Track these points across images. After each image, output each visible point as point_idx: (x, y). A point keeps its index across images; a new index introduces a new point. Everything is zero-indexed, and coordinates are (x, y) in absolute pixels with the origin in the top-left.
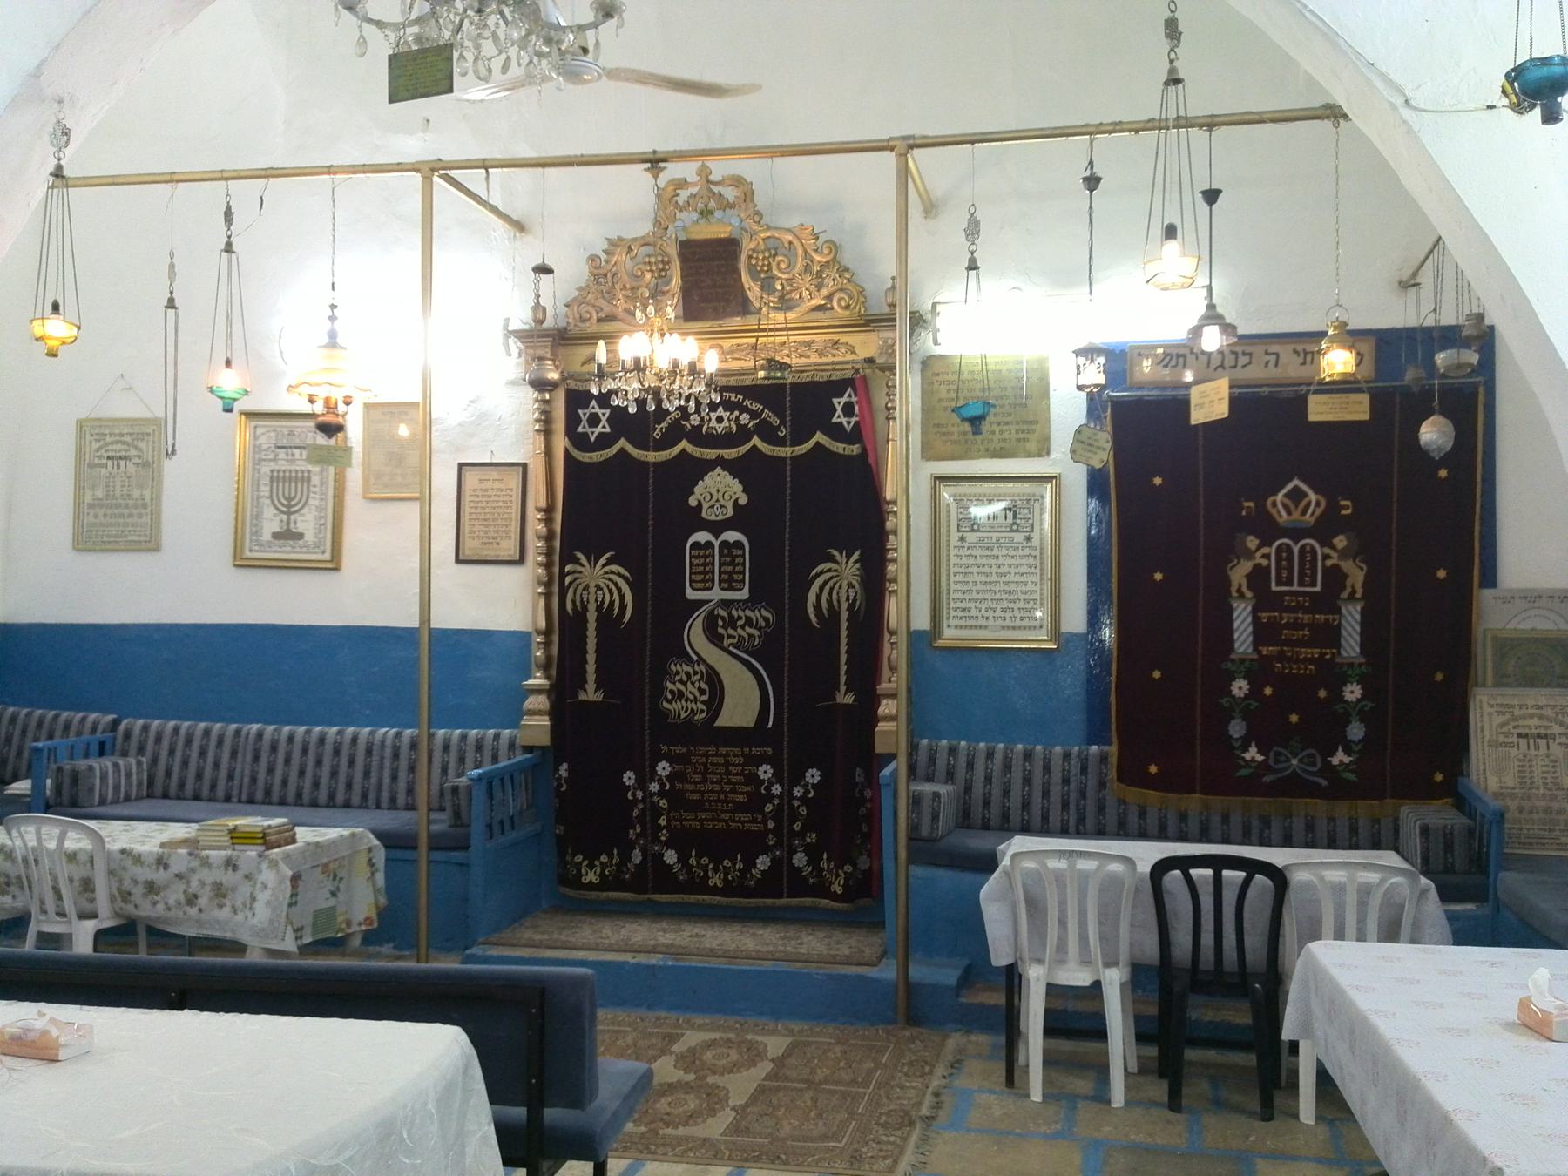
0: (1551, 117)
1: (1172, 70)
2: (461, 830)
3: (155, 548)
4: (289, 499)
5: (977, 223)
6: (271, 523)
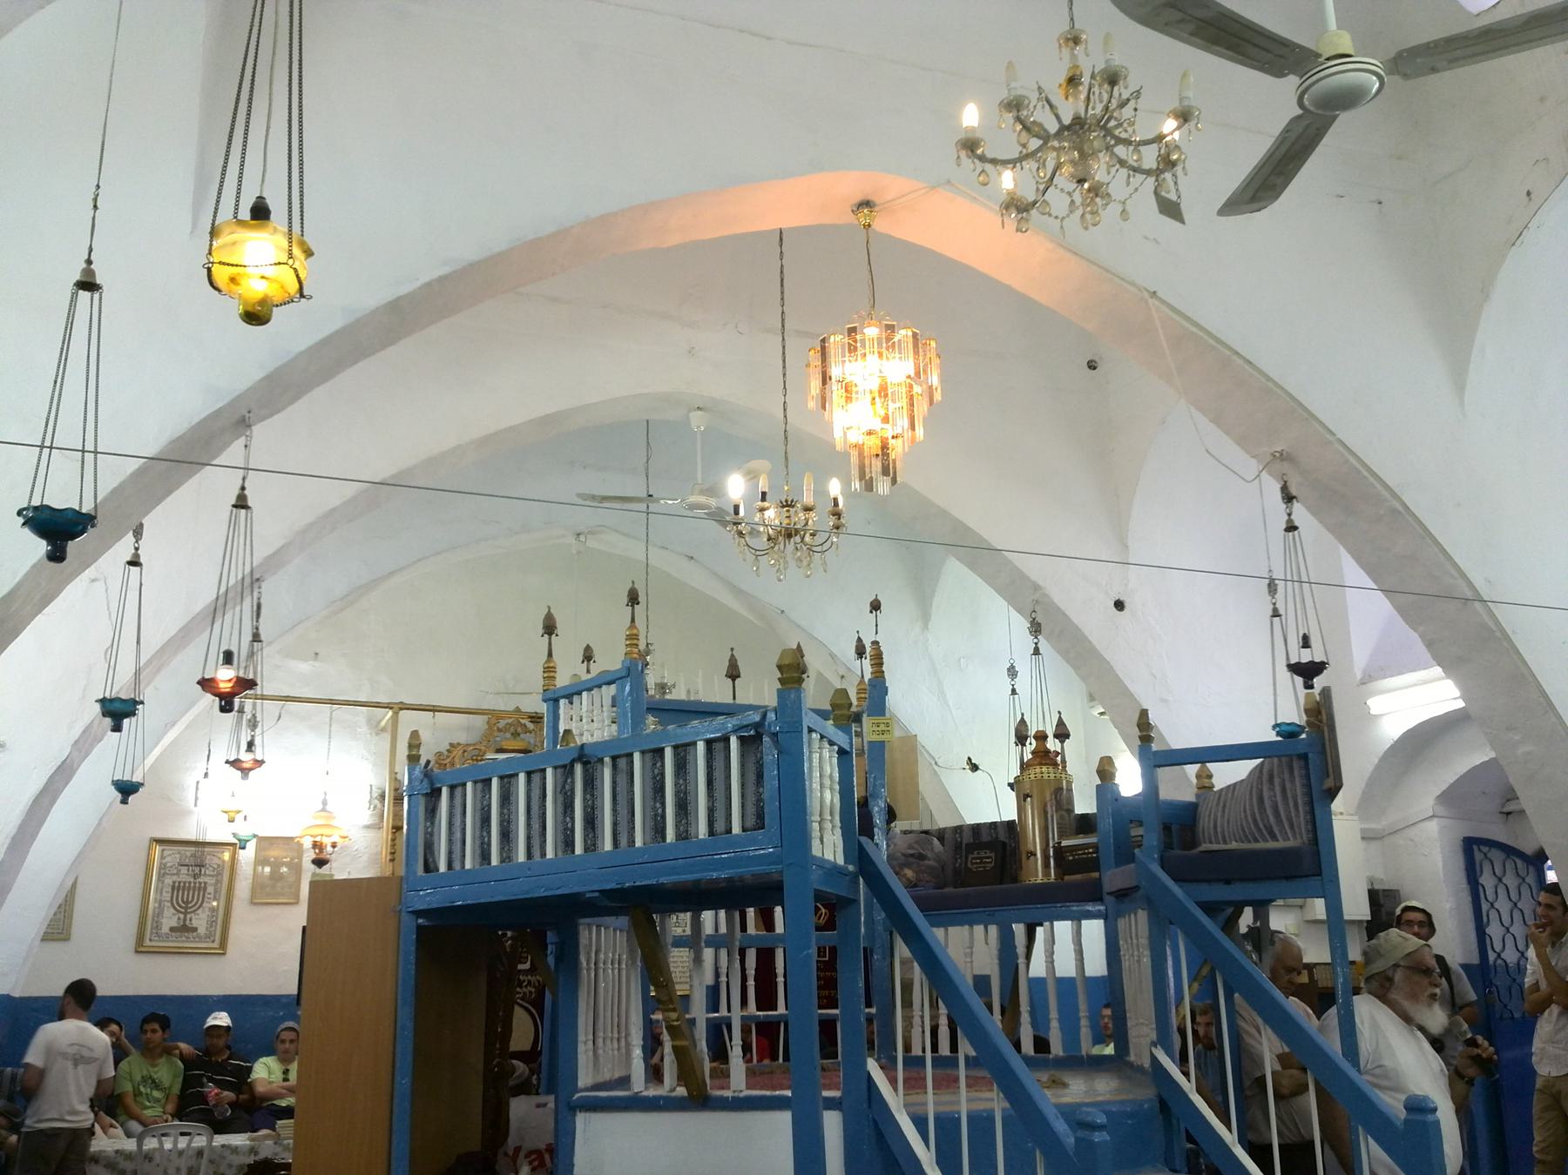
0: (117, 728)
1: (1290, 521)
2: (1046, 771)
3: (67, 939)
4: (187, 903)
6: (170, 920)
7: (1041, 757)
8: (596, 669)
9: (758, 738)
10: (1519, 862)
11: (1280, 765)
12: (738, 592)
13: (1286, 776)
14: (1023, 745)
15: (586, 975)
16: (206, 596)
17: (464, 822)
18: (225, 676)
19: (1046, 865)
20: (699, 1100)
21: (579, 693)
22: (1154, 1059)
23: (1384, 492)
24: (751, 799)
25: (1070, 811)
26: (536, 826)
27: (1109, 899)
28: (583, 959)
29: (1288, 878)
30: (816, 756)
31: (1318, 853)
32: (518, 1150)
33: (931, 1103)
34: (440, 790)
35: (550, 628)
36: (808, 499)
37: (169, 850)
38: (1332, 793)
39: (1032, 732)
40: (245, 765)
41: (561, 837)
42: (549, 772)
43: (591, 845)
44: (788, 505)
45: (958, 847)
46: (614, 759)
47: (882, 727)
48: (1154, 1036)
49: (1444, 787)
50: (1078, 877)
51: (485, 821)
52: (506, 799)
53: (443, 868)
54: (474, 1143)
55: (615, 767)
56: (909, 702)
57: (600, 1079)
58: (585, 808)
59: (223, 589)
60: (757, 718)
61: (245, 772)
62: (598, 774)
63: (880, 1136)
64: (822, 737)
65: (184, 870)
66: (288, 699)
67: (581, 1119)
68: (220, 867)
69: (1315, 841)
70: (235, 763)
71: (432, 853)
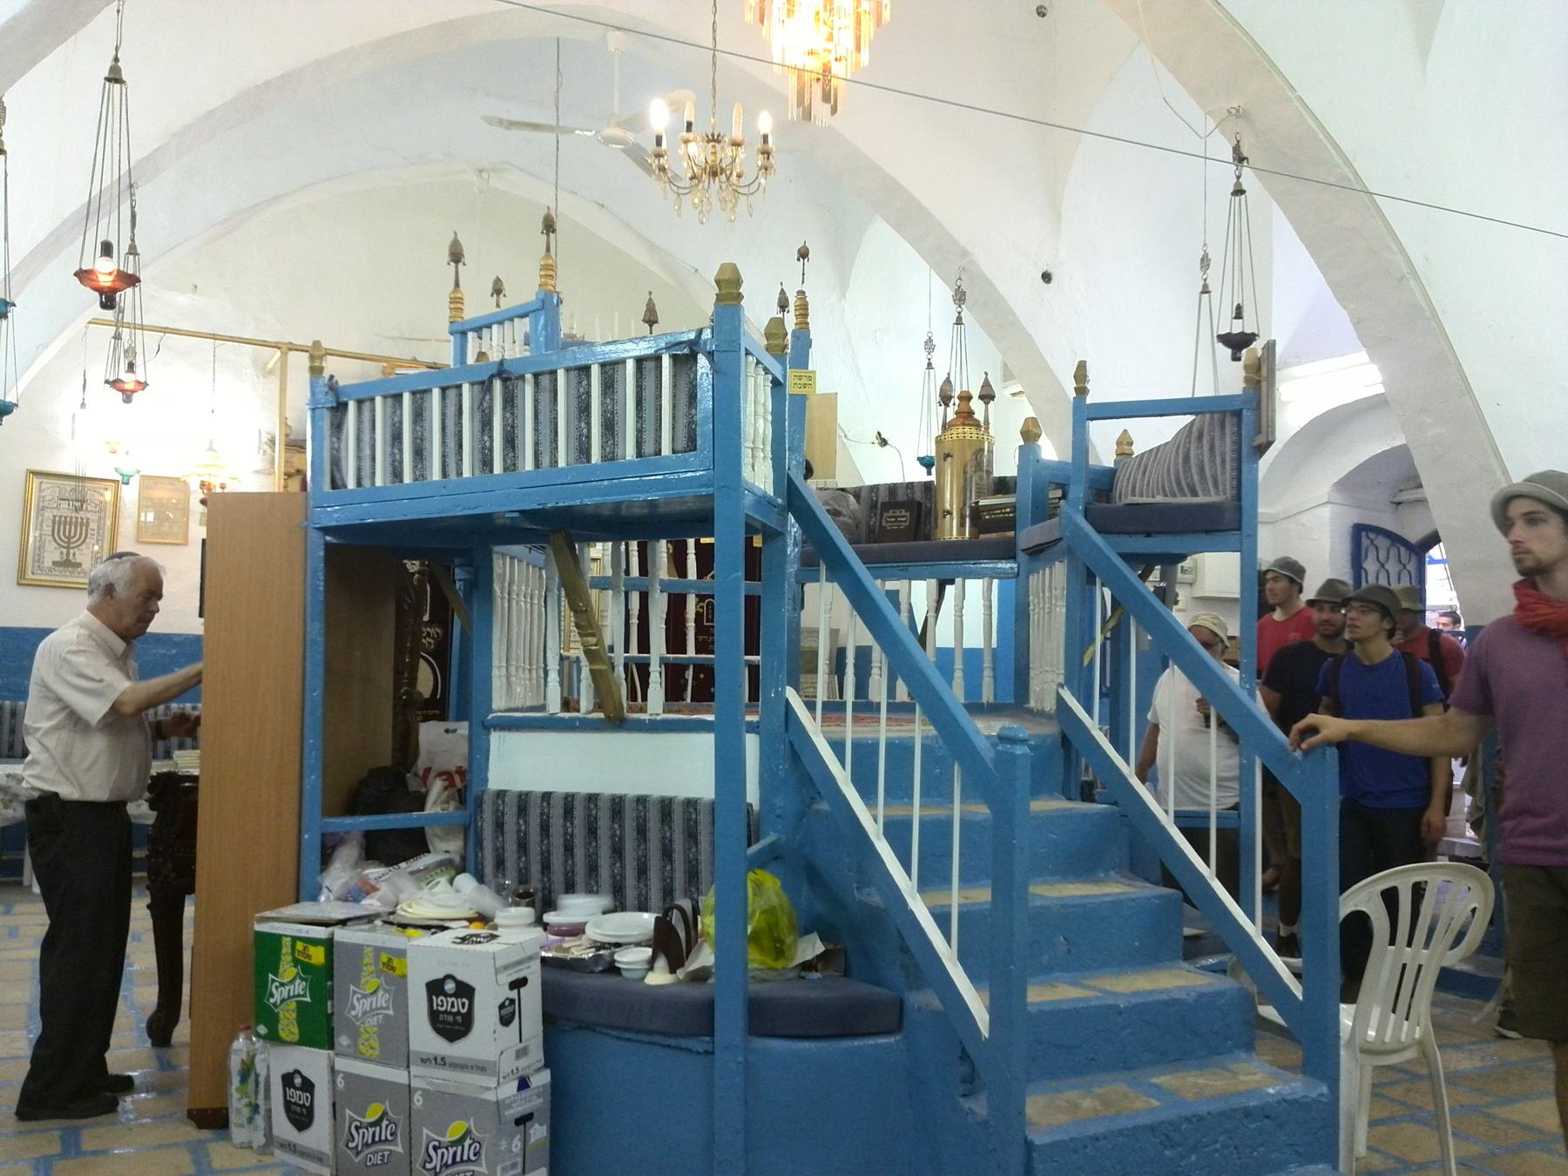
1: (1238, 184)
2: (969, 432)
5: (964, 293)
6: (52, 554)
7: (962, 412)
8: (506, 303)
9: (692, 358)
10: (1403, 550)
11: (1212, 423)
12: (652, 247)
13: (1217, 434)
14: (947, 405)
15: (500, 603)
16: (77, 199)
17: (373, 439)
18: (105, 270)
19: (962, 524)
20: (616, 722)
21: (489, 326)
22: (1060, 699)
23: (1336, 157)
24: (682, 421)
25: (989, 472)
26: (452, 444)
27: (1022, 556)
28: (497, 587)
29: (1207, 532)
30: (751, 381)
31: (1239, 509)
32: (428, 770)
33: (849, 731)
34: (345, 405)
35: (456, 256)
36: (737, 134)
37: (47, 483)
38: (1261, 449)
39: (957, 393)
40: (127, 387)
41: (478, 456)
42: (466, 388)
43: (511, 466)
44: (714, 139)
45: (873, 505)
46: (536, 376)
47: (804, 380)
48: (1061, 680)
49: (1342, 474)
50: (994, 535)
51: (397, 437)
52: (419, 415)
53: (351, 484)
54: (385, 758)
55: (537, 384)
56: (829, 368)
57: (513, 705)
58: (505, 426)
59: (96, 192)
60: (692, 336)
61: (128, 396)
62: (518, 392)
63: (795, 757)
64: (758, 362)
65: (64, 504)
66: (166, 330)
67: (495, 737)
68: (101, 507)
69: (1238, 497)
70: (115, 384)
71: (340, 470)
